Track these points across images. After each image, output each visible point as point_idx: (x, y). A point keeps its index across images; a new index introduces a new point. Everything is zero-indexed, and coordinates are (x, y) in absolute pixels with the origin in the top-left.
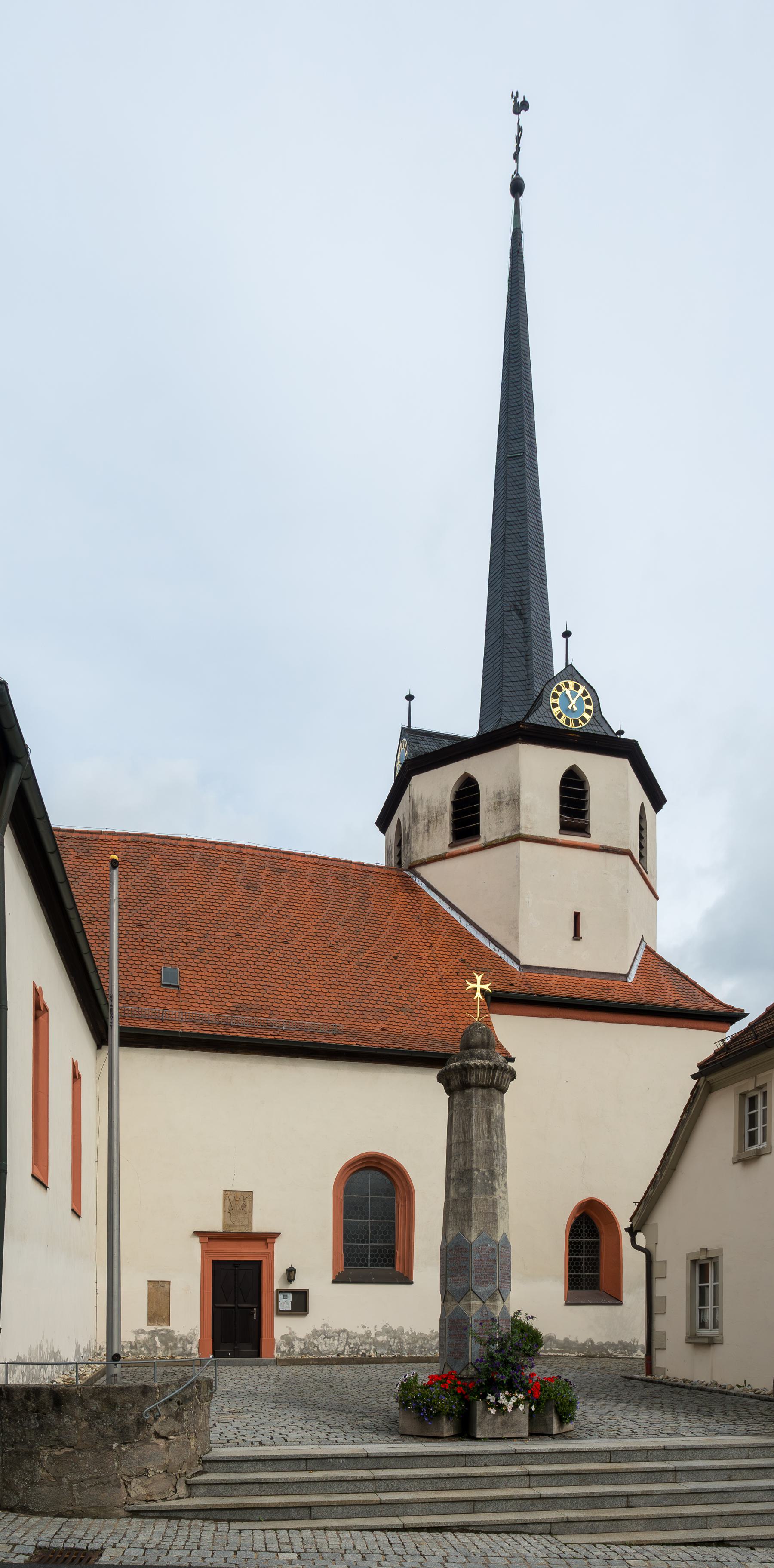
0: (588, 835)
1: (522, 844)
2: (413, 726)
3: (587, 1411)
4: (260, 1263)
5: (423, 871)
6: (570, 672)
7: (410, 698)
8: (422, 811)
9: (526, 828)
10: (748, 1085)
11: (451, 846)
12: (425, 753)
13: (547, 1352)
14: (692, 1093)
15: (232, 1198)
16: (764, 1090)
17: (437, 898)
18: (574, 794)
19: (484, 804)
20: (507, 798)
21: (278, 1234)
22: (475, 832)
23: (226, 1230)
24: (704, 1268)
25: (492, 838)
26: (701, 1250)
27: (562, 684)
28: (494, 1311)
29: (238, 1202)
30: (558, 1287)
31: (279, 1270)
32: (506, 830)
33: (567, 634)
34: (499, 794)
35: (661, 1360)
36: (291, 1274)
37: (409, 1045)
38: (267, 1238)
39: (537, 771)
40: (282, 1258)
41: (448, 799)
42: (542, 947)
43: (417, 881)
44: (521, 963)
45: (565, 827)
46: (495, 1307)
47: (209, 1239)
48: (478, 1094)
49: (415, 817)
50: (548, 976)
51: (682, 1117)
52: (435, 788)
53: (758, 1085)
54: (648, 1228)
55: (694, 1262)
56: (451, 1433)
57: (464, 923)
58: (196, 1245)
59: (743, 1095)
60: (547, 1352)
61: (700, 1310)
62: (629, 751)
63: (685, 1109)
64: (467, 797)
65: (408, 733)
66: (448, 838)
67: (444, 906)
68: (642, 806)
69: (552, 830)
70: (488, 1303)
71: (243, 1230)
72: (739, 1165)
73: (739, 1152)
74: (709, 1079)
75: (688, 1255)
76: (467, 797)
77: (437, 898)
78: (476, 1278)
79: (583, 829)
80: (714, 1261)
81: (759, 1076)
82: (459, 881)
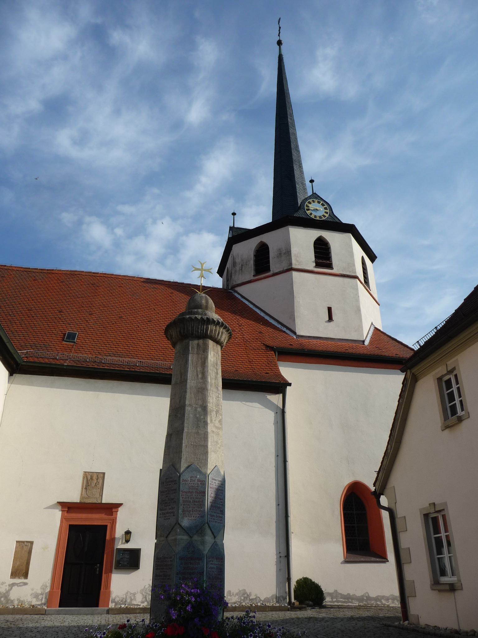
0: (332, 268)
1: (295, 274)
2: (236, 226)
4: (105, 527)
5: (239, 289)
6: (315, 196)
7: (234, 214)
8: (238, 260)
9: (296, 265)
10: (440, 370)
11: (254, 276)
13: (334, 602)
14: (403, 383)
15: (89, 477)
16: (454, 373)
17: (247, 303)
18: (322, 252)
19: (272, 255)
20: (284, 251)
21: (120, 505)
22: (268, 269)
23: (83, 501)
24: (434, 521)
25: (277, 271)
26: (430, 504)
27: (311, 200)
28: (201, 547)
29: (94, 480)
30: (338, 548)
31: (119, 532)
32: (285, 266)
33: (312, 181)
35: (414, 608)
38: (111, 509)
39: (301, 240)
40: (122, 523)
41: (252, 254)
42: (309, 324)
43: (236, 294)
44: (297, 334)
45: (318, 265)
46: (203, 543)
47: (69, 508)
48: (194, 343)
49: (234, 264)
50: (315, 341)
51: (399, 401)
52: (246, 250)
53: (449, 369)
54: (387, 491)
55: (426, 516)
57: (262, 314)
58: (58, 514)
59: (440, 380)
60: (334, 602)
61: (438, 558)
62: (351, 229)
63: (400, 396)
64: (262, 253)
65: (232, 229)
66: (253, 273)
67: (251, 306)
68: (363, 258)
69: (311, 266)
70: (195, 538)
71: (95, 501)
72: (447, 431)
73: (445, 420)
74: (413, 371)
75: (421, 510)
76: (262, 253)
77: (247, 303)
78: (183, 511)
79: (330, 266)
80: (443, 513)
81: (448, 363)
82: (258, 293)
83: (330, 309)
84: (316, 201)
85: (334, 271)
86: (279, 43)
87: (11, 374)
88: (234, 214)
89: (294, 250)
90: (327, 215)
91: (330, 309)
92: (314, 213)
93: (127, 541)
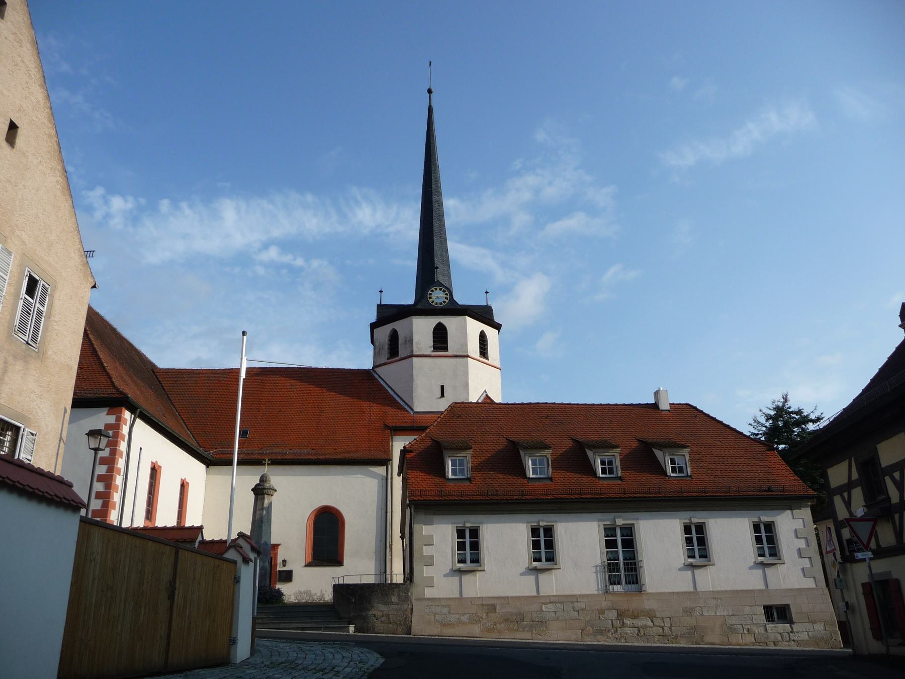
1: (415, 360)
3: (606, 612)
7: (381, 292)
12: (388, 315)
18: (440, 338)
19: (400, 341)
31: (280, 560)
34: (406, 337)
36: (284, 562)
37: (355, 457)
39: (422, 329)
45: (436, 348)
50: (427, 415)
56: (874, 572)
57: (392, 393)
65: (381, 307)
69: (429, 350)
77: (382, 382)
82: (390, 375)
83: (442, 387)
84: (438, 288)
85: (450, 353)
86: (430, 91)
87: (207, 467)
88: (381, 292)
89: (416, 339)
90: (447, 301)
91: (442, 387)
92: (436, 301)
93: (284, 566)
